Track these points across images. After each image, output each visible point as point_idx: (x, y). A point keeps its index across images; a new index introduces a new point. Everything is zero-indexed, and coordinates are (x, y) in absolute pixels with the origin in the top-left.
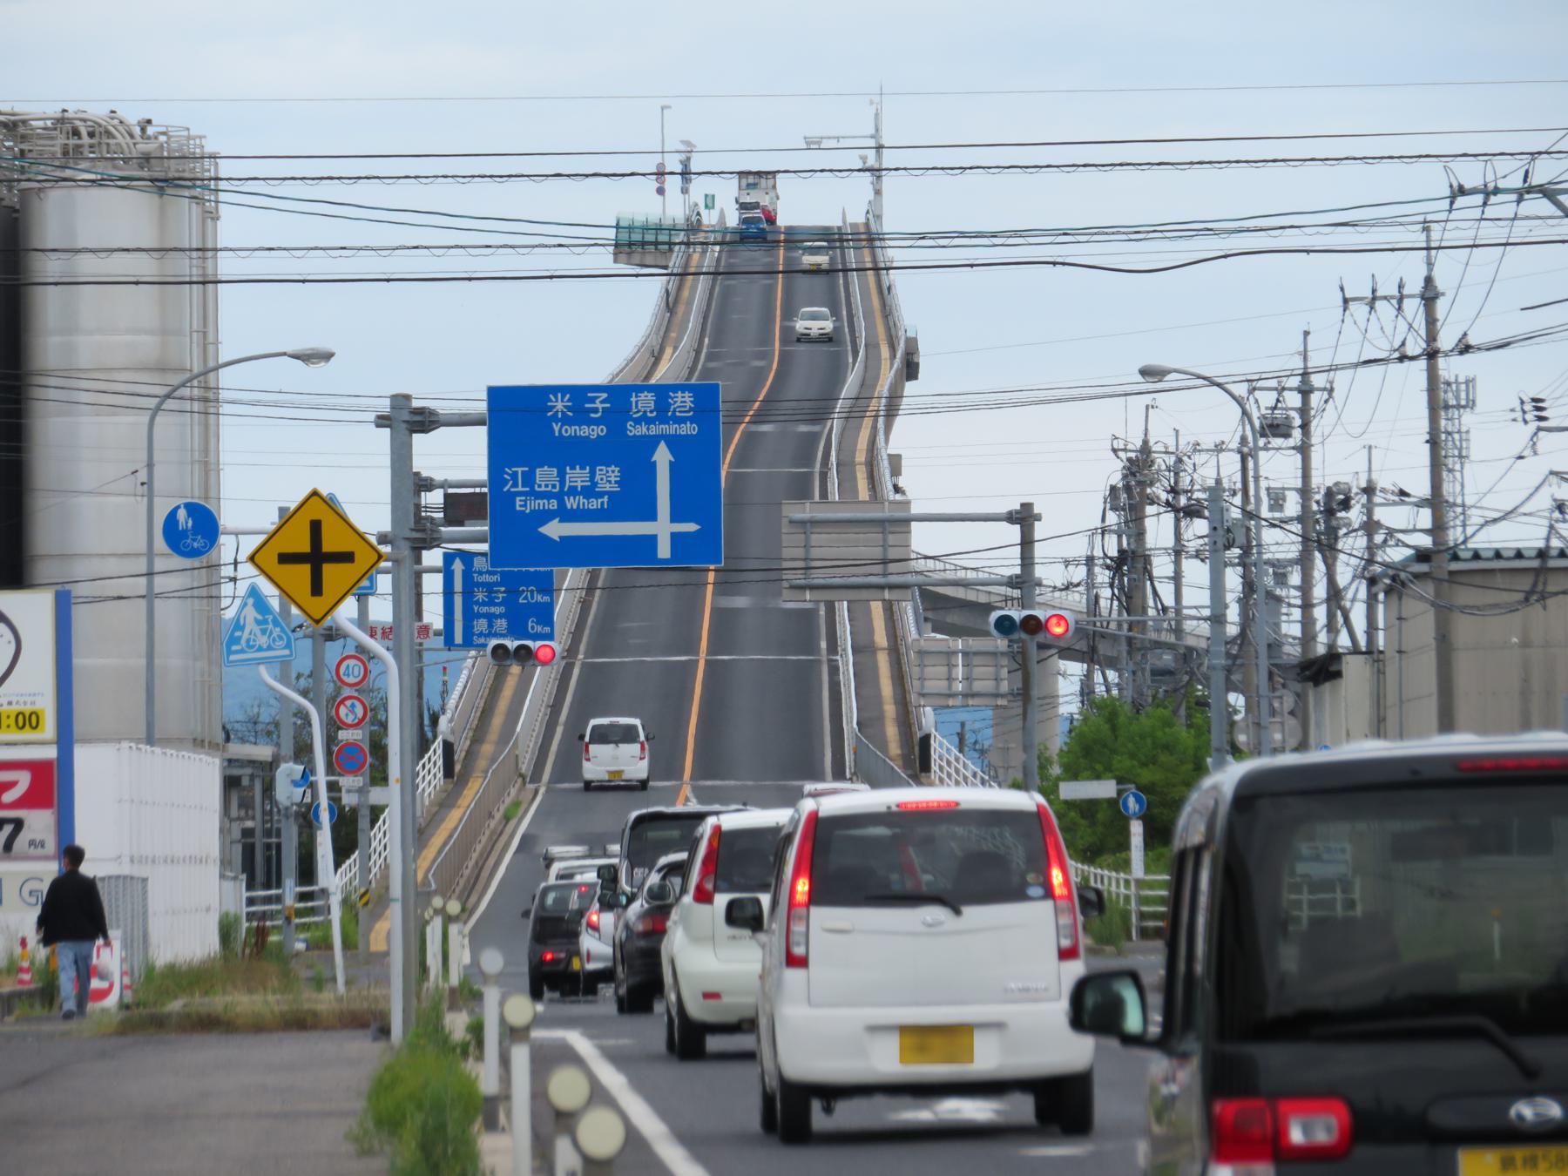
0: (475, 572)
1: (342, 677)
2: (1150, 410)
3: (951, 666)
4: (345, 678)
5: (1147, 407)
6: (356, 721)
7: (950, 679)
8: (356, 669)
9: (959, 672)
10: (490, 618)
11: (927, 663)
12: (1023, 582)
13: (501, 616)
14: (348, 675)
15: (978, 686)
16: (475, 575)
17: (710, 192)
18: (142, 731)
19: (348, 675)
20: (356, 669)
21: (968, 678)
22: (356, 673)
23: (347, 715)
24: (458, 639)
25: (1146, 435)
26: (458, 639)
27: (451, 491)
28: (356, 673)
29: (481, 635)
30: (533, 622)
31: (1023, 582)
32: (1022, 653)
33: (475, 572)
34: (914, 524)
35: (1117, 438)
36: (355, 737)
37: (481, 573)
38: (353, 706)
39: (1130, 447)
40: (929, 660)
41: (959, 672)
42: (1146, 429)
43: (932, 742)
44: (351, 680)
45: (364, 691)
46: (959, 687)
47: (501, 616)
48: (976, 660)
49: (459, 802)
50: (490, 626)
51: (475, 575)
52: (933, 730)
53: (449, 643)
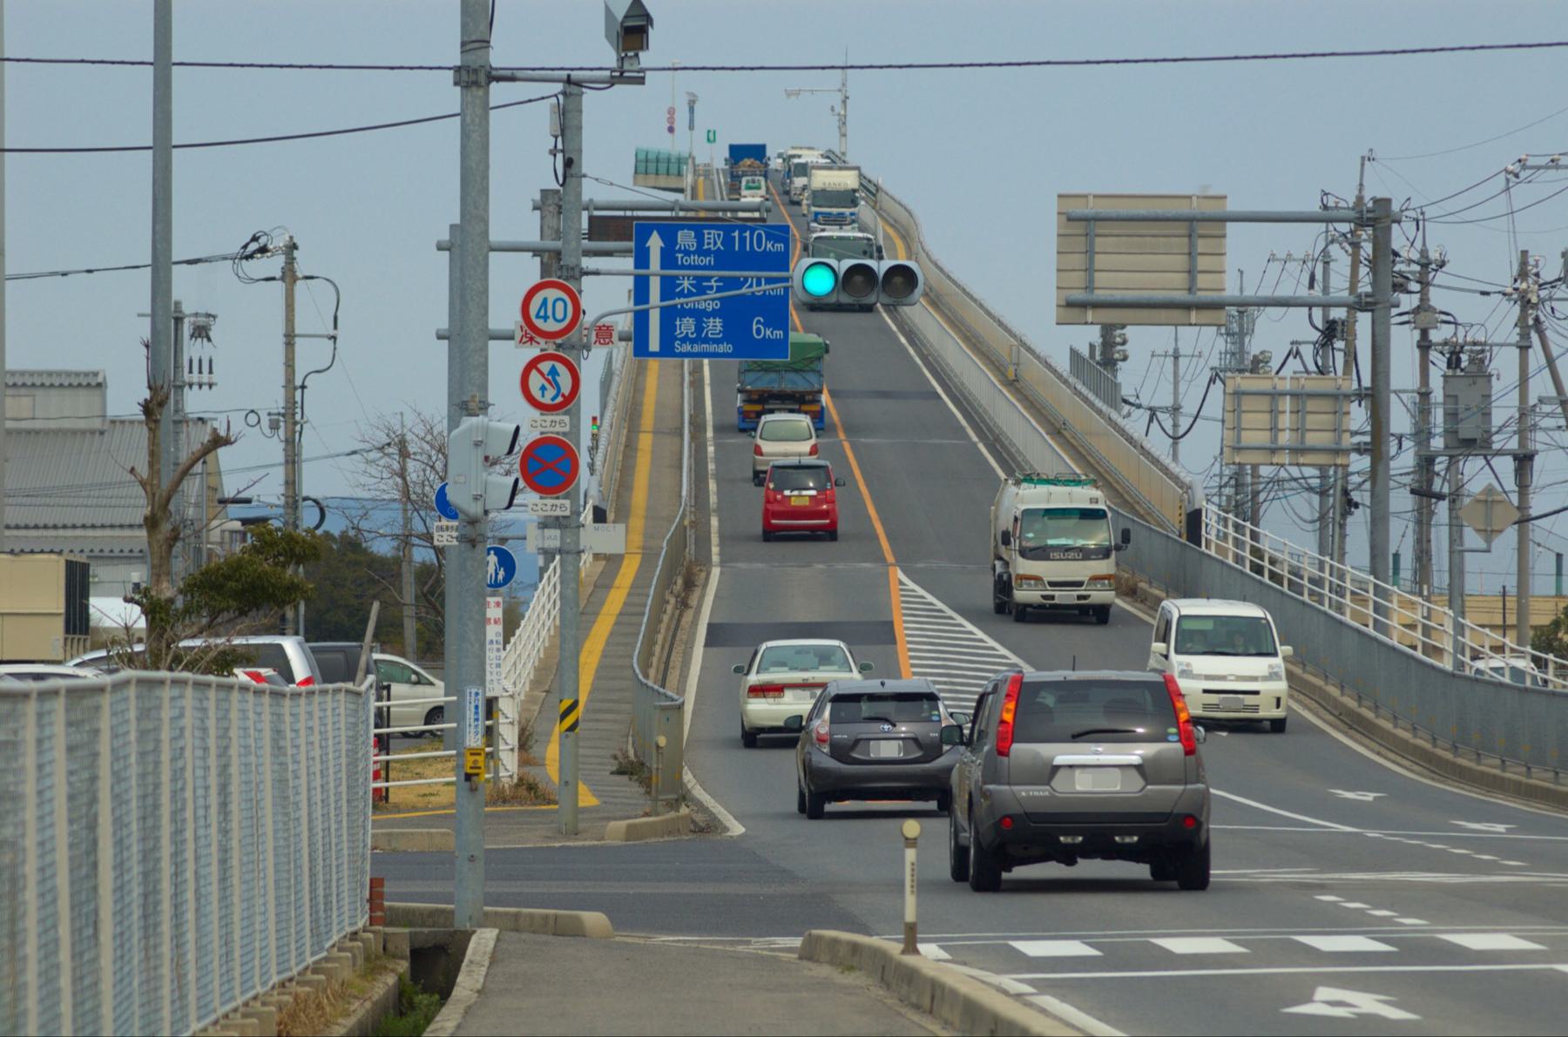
0: (680, 251)
1: (533, 316)
2: (1367, 162)
3: (1274, 412)
4: (539, 323)
5: (1363, 158)
6: (560, 399)
7: (1274, 429)
8: (560, 305)
9: (1286, 420)
10: (699, 315)
11: (1244, 408)
12: (1375, 304)
13: (714, 314)
14: (545, 318)
15: (1312, 439)
16: (680, 256)
17: (712, 129)
18: (97, 392)
19: (545, 318)
20: (560, 305)
21: (1300, 429)
22: (559, 315)
23: (543, 388)
24: (654, 344)
25: (1360, 190)
26: (654, 344)
27: (597, 213)
28: (559, 315)
29: (685, 339)
30: (759, 322)
31: (1375, 304)
32: (1372, 396)
33: (680, 251)
34: (1231, 227)
35: (1326, 194)
36: (558, 428)
37: (687, 253)
38: (553, 371)
39: (1342, 204)
40: (1247, 403)
41: (1286, 420)
42: (1361, 184)
43: (1204, 518)
44: (551, 326)
45: (573, 347)
46: (1285, 438)
47: (714, 314)
48: (1311, 405)
49: (617, 582)
50: (699, 328)
51: (680, 256)
52: (1204, 503)
53: (641, 349)
